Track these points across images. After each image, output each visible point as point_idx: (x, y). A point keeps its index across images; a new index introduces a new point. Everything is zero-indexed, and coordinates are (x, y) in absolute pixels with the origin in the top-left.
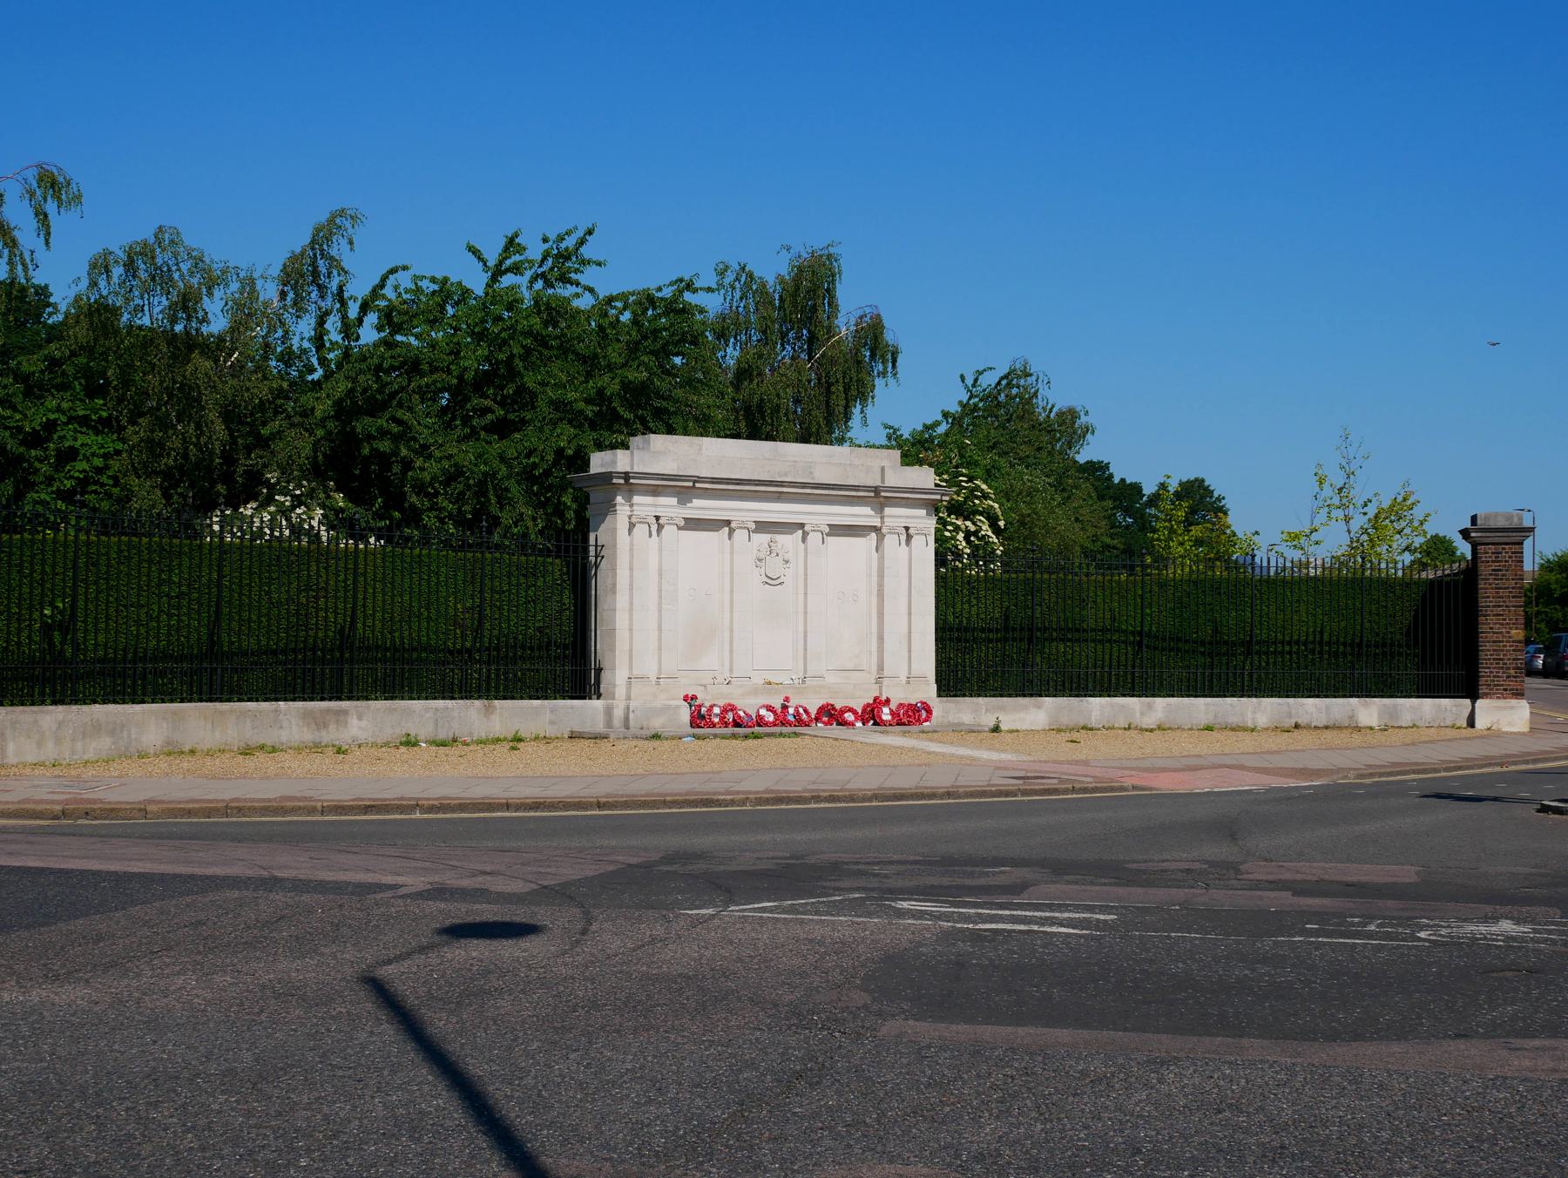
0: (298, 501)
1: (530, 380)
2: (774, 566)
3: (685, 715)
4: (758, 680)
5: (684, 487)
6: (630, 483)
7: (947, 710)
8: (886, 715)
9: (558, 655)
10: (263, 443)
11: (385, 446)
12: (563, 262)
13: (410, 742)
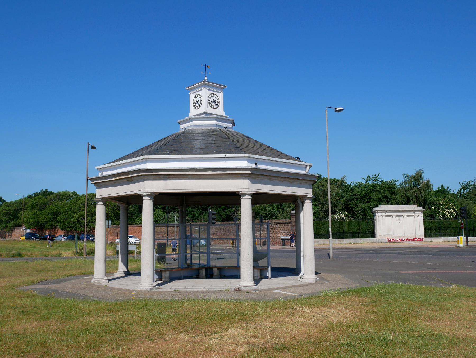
0: (341, 214)
1: (371, 195)
2: (399, 221)
3: (387, 240)
4: (398, 235)
5: (386, 212)
6: (378, 212)
7: (425, 239)
8: (416, 240)
9: (372, 234)
10: (336, 206)
11: (352, 206)
12: (376, 178)
13: (351, 243)
